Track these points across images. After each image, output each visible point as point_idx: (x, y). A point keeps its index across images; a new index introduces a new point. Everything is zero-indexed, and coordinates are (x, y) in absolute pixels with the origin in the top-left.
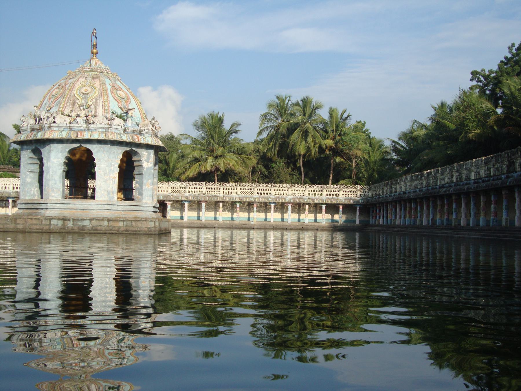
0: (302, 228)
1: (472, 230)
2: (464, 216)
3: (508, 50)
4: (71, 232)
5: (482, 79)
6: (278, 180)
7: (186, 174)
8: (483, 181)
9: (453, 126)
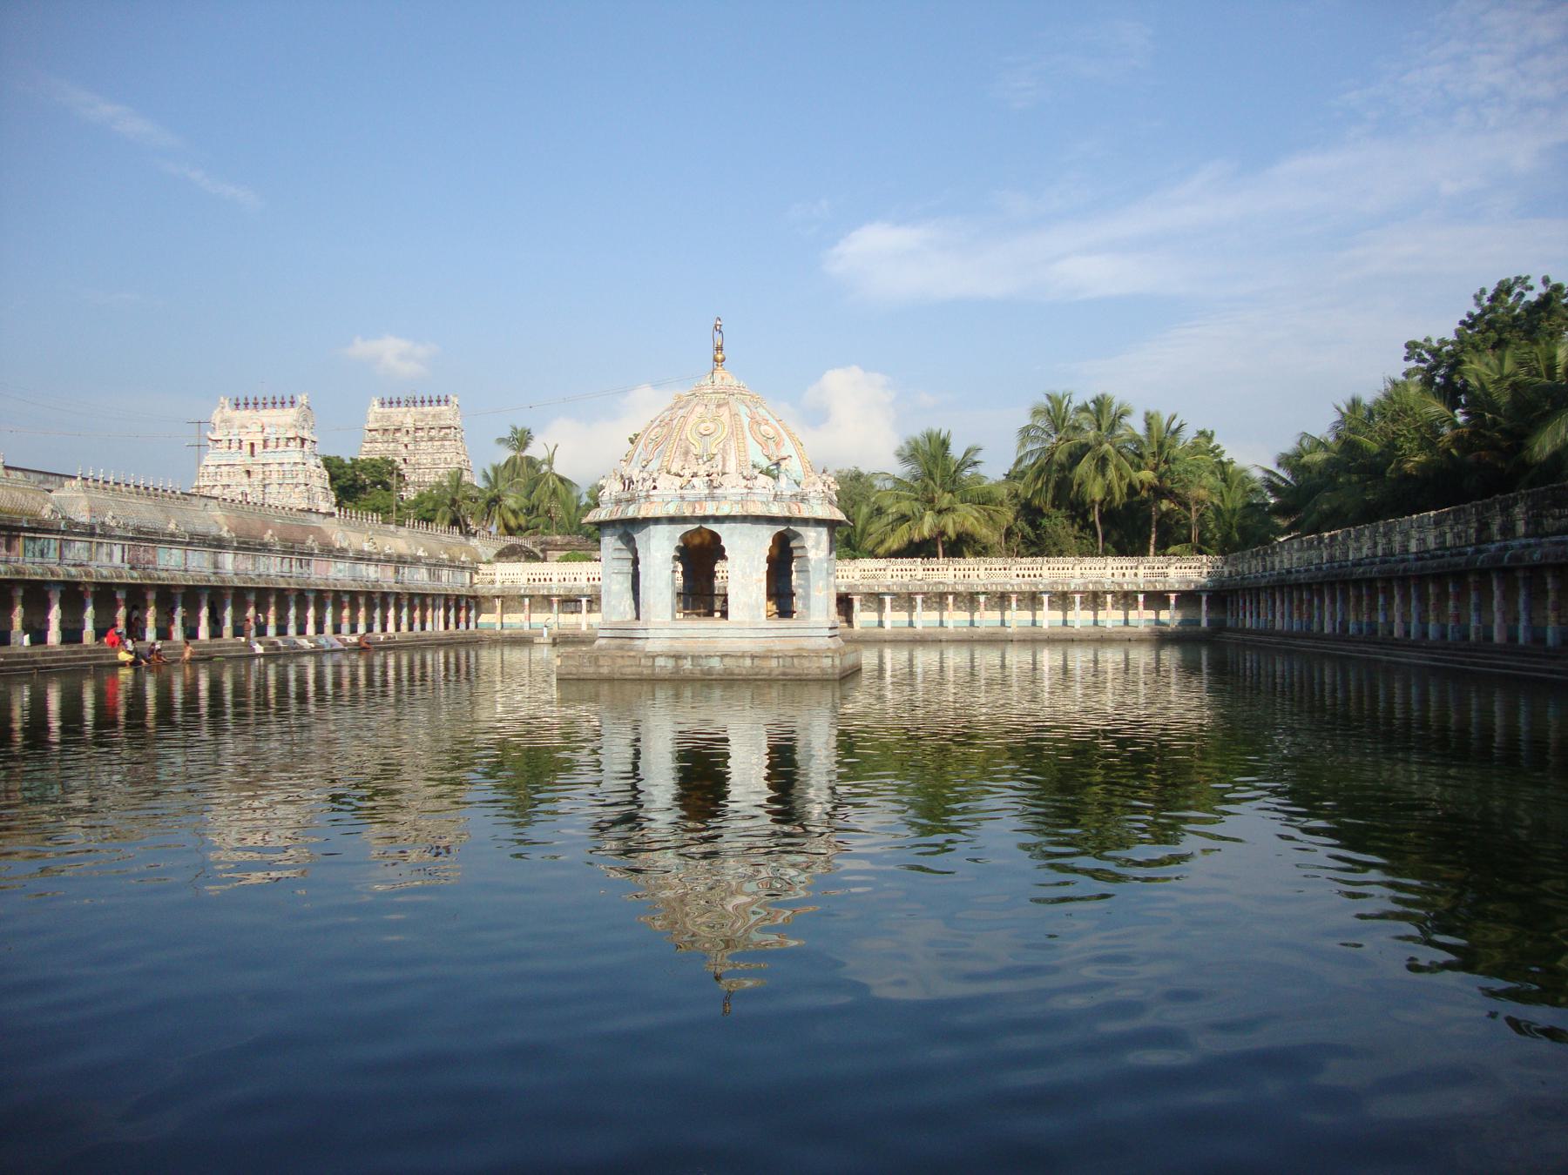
0: (1103, 640)
1: (1413, 646)
2: (1398, 616)
3: (1473, 301)
4: (691, 680)
5: (1427, 356)
6: (1054, 550)
7: (886, 545)
8: (1433, 557)
9: (1374, 447)
